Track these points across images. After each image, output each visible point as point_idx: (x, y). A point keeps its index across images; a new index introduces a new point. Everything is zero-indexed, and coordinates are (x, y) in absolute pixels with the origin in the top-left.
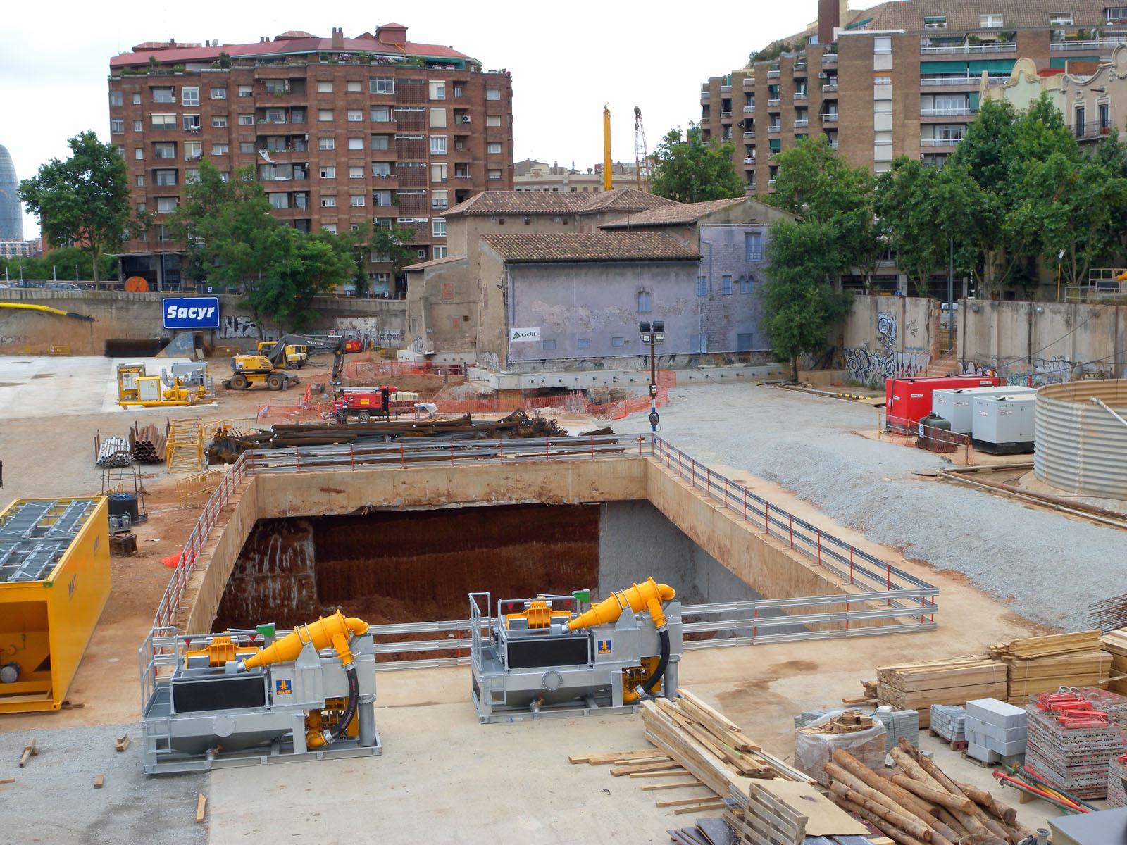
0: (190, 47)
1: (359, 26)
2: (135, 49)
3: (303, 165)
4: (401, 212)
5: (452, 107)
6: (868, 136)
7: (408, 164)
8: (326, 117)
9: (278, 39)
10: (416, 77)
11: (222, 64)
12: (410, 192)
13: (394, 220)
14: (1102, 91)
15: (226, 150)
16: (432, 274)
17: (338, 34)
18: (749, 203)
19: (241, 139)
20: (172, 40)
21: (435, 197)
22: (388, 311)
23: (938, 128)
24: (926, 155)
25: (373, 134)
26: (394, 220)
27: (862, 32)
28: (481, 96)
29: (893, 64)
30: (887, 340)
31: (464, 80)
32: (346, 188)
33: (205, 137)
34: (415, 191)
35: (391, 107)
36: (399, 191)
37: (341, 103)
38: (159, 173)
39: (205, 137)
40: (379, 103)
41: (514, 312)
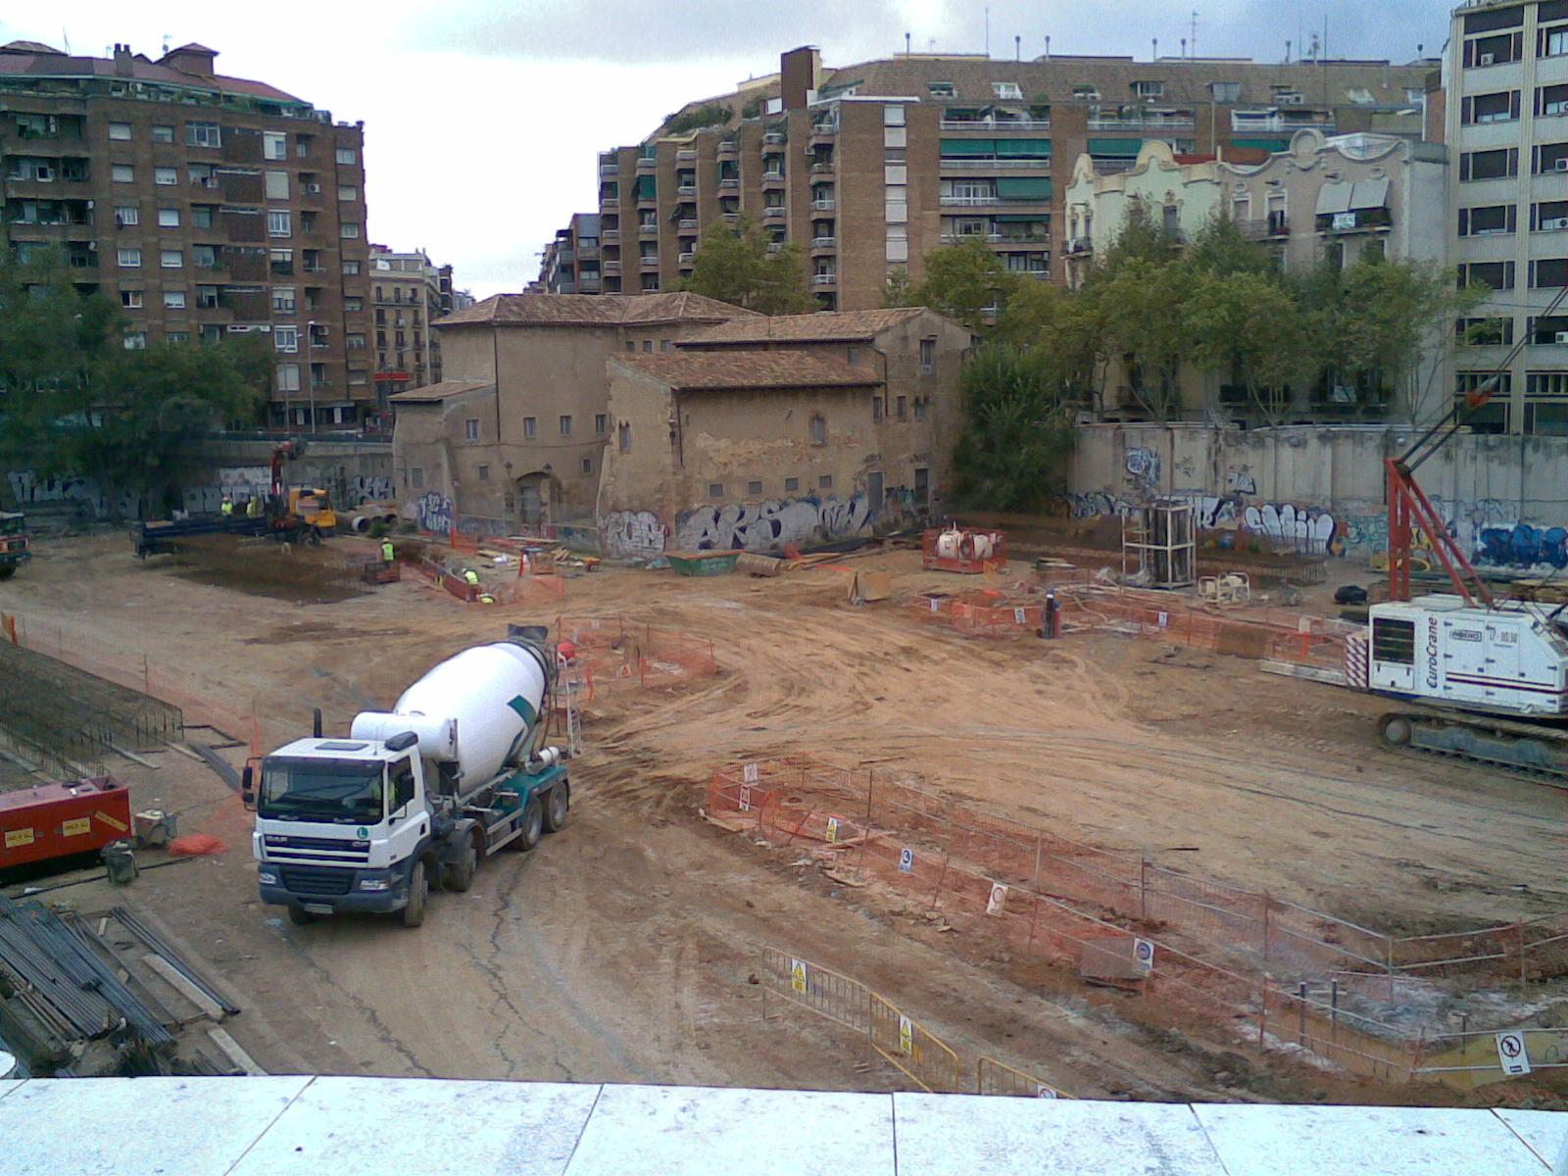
5: (297, 171)
6: (878, 229)
7: (239, 249)
8: (123, 176)
10: (248, 126)
12: (246, 289)
13: (222, 328)
16: (453, 406)
18: (925, 315)
21: (277, 295)
23: (957, 220)
25: (193, 205)
26: (222, 328)
30: (1142, 482)
31: (310, 132)
35: (213, 166)
37: (144, 156)
40: (200, 160)
41: (46, 515)
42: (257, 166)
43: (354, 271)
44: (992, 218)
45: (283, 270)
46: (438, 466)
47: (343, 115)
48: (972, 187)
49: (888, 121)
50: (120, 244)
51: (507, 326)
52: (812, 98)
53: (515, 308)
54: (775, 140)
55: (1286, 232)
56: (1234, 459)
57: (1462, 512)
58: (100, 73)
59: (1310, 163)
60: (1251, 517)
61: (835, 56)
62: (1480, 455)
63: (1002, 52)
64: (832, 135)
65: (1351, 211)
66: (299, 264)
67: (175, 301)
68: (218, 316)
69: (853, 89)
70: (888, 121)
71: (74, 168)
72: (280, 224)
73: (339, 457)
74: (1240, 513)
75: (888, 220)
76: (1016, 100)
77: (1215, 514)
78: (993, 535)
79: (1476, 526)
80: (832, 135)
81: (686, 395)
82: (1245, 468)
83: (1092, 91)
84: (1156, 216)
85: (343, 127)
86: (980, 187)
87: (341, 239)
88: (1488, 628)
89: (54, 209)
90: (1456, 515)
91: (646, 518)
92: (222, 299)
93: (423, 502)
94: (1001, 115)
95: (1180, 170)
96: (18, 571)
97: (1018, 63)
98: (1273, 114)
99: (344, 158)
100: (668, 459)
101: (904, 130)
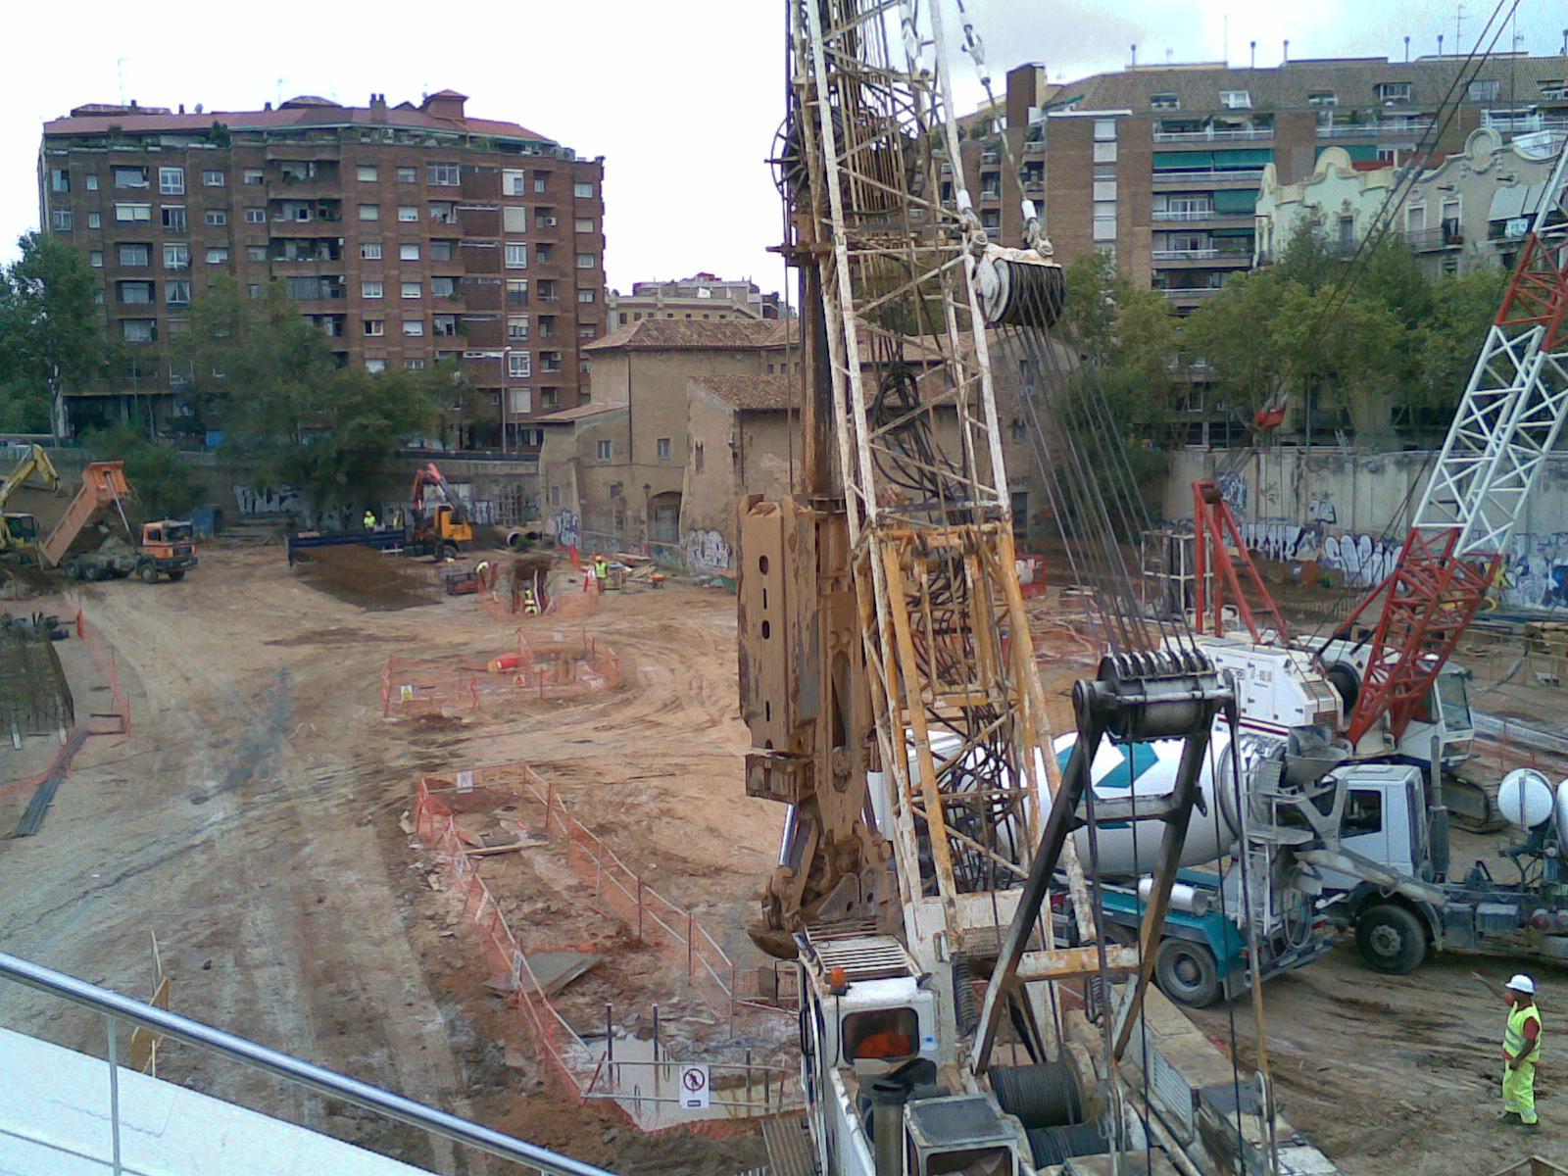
0: (155, 112)
1: (406, 89)
2: (74, 113)
3: (334, 279)
4: (470, 345)
9: (286, 106)
11: (214, 135)
12: (482, 317)
14: (1449, 189)
15: (225, 256)
16: (585, 427)
17: (378, 101)
19: (249, 242)
20: (134, 102)
21: (512, 323)
22: (486, 476)
23: (1172, 236)
24: (1158, 270)
25: (432, 240)
27: (1067, 113)
28: (567, 186)
29: (1119, 155)
32: (397, 311)
33: (193, 238)
34: (485, 316)
35: (454, 203)
36: (465, 316)
37: (388, 196)
38: (124, 285)
39: (193, 238)
42: (495, 202)
43: (589, 299)
44: (1210, 232)
45: (520, 300)
46: (569, 484)
47: (586, 152)
48: (1188, 201)
49: (1098, 136)
50: (363, 277)
51: (640, 350)
52: (1035, 116)
53: (655, 333)
54: (990, 160)
55: (1460, 241)
56: (1316, 487)
57: (1535, 546)
58: (358, 121)
59: (1486, 166)
60: (1330, 547)
61: (1062, 71)
62: (1552, 484)
63: (1239, 60)
64: (1043, 152)
65: (1524, 216)
66: (533, 295)
67: (415, 329)
68: (456, 344)
69: (1074, 105)
70: (1098, 136)
71: (329, 209)
72: (516, 257)
73: (522, 475)
74: (1320, 543)
75: (1096, 237)
76: (1247, 109)
77: (1296, 544)
78: (1031, 562)
79: (1548, 562)
80: (1043, 152)
81: (747, 416)
82: (1326, 496)
83: (1331, 96)
84: (1330, 230)
85: (583, 163)
86: (1197, 200)
87: (576, 269)
88: (1250, 666)
89: (312, 246)
90: (1528, 550)
91: (715, 537)
92: (459, 327)
93: (559, 519)
94: (1219, 125)
95: (1356, 177)
96: (187, 575)
97: (1252, 69)
98: (1533, 112)
99: (583, 192)
100: (731, 479)
101: (1114, 145)
